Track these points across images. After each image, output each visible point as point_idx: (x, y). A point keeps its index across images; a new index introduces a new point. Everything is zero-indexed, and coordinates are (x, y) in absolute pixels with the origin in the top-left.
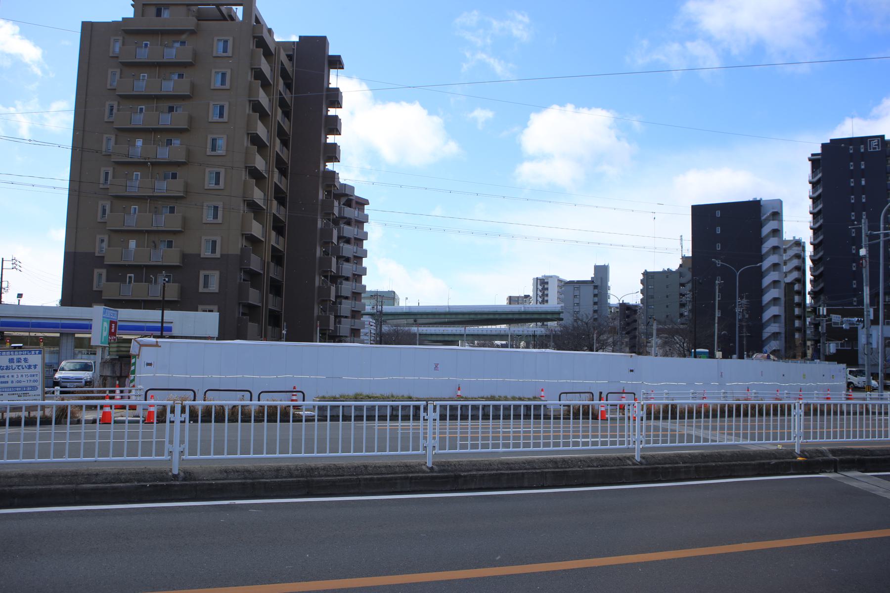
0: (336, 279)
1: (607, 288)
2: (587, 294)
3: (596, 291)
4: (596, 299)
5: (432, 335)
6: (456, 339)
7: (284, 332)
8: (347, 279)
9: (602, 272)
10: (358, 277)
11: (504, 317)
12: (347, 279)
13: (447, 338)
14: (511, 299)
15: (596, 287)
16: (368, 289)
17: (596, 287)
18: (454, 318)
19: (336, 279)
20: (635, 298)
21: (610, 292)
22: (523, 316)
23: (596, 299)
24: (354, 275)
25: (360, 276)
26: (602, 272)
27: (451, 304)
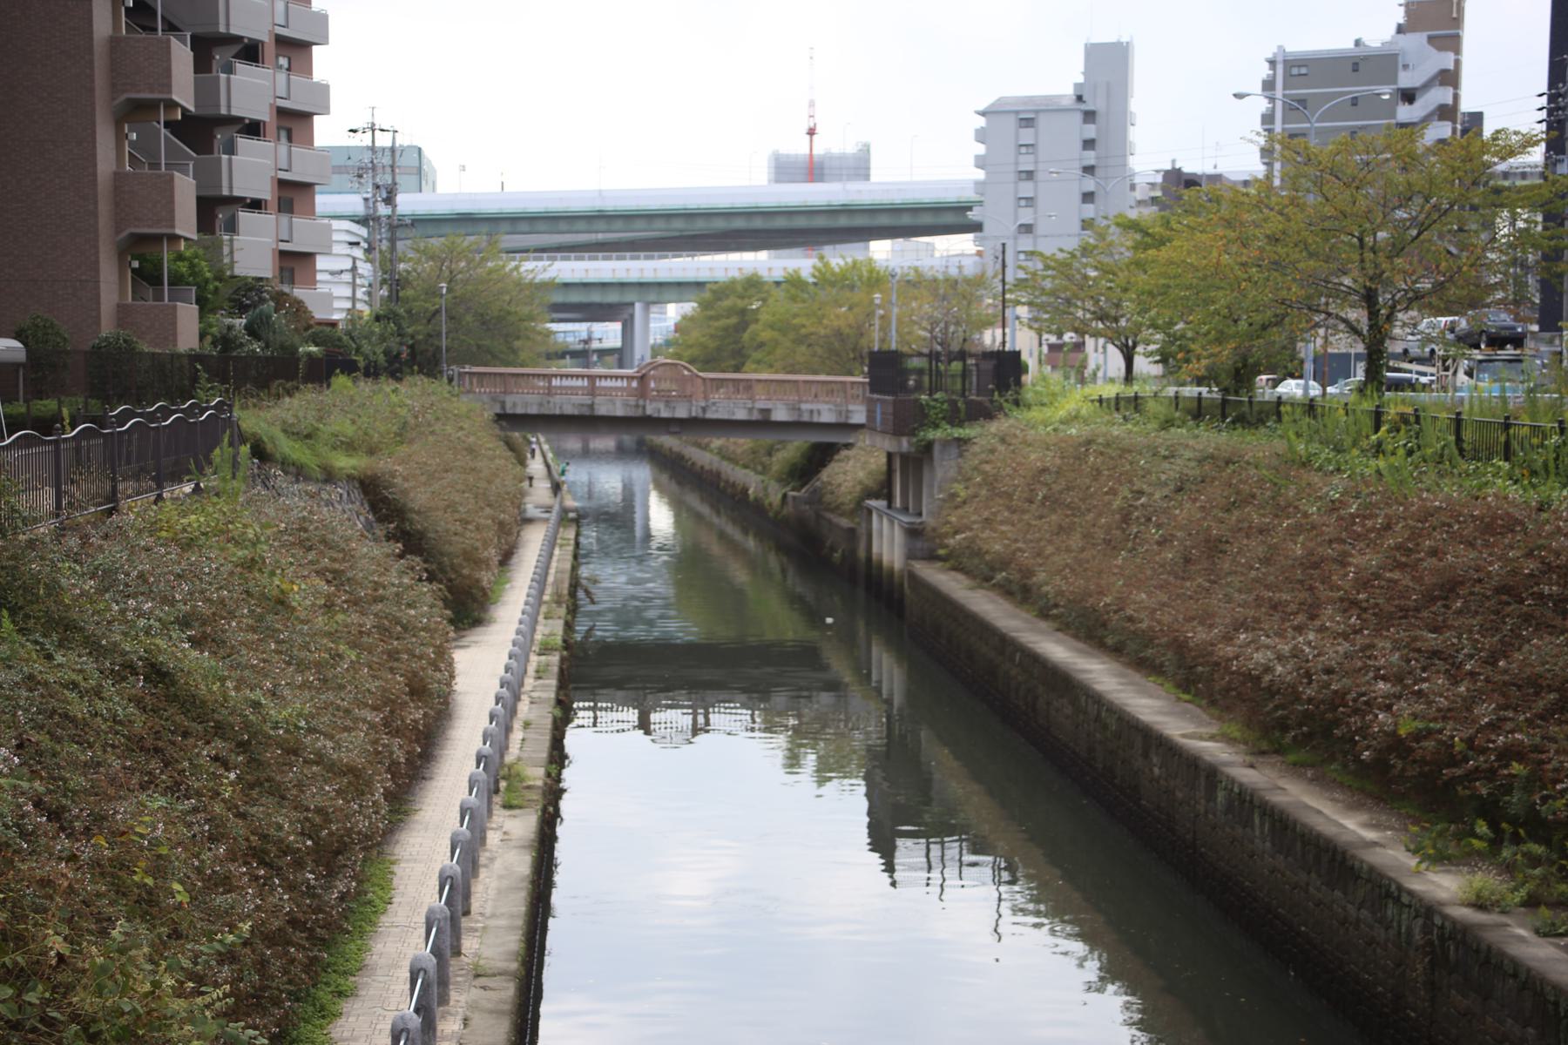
0: (204, 131)
1: (1123, 119)
2: (1061, 144)
3: (1090, 131)
4: (1090, 157)
5: (567, 285)
6: (628, 298)
7: (1155, 760)
8: (253, 129)
9: (1109, 64)
10: (294, 122)
11: (781, 223)
12: (253, 129)
13: (596, 297)
14: (784, 169)
15: (1089, 116)
16: (1081, 79)
17: (1089, 116)
18: (657, 230)
19: (204, 131)
20: (1233, 149)
21: (1135, 135)
22: (843, 221)
23: (1090, 157)
24: (282, 113)
25: (305, 117)
26: (1109, 64)
27: (916, 178)
